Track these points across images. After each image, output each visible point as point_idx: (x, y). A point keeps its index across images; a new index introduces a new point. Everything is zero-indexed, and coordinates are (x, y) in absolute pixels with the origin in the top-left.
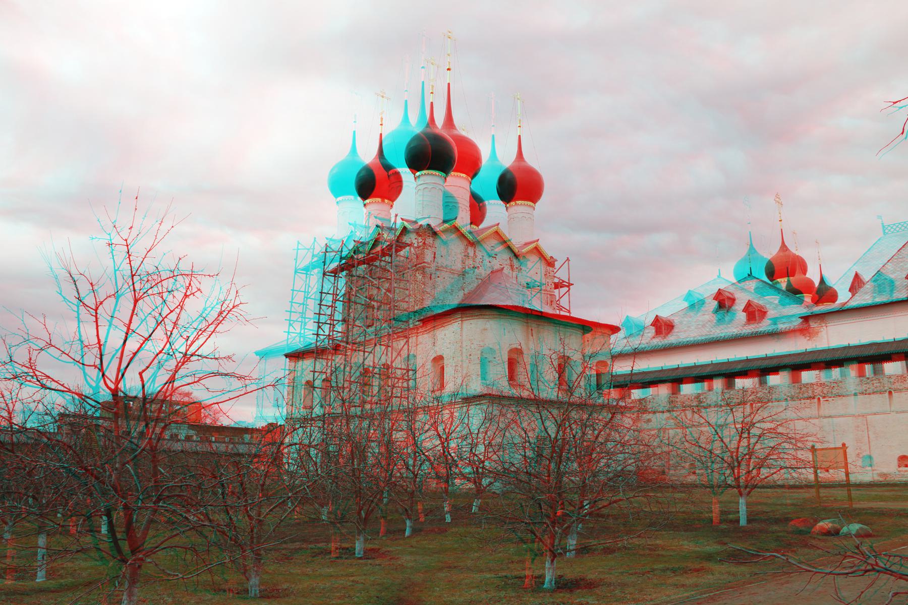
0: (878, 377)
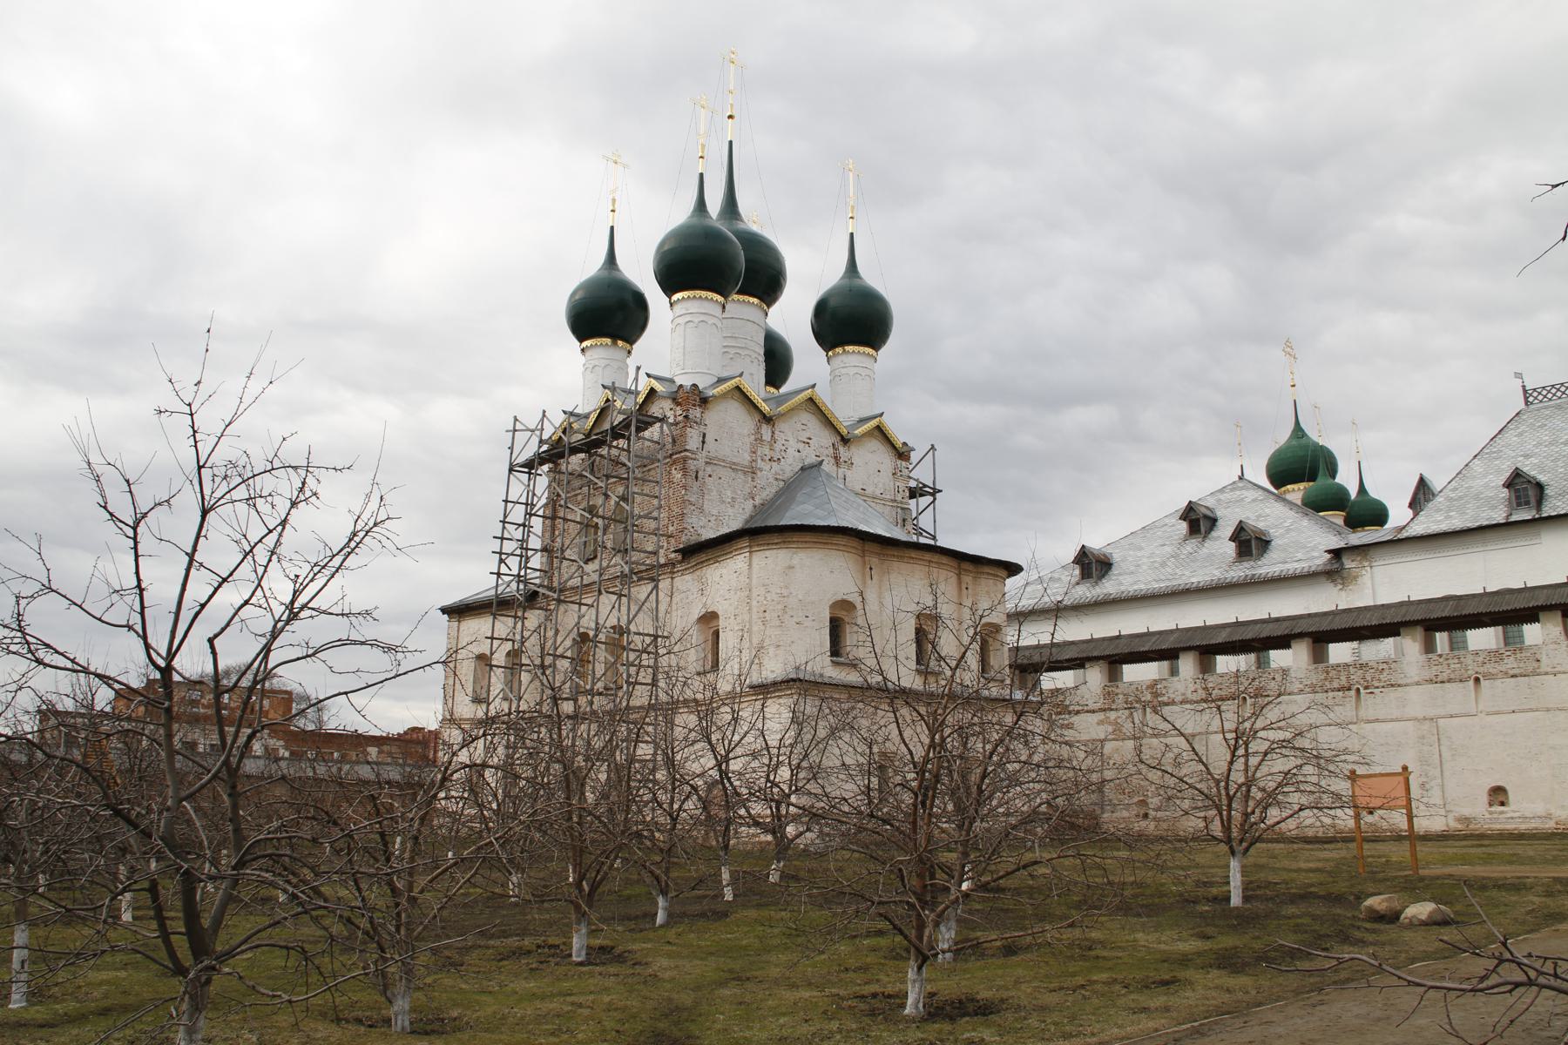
0: (1456, 653)
